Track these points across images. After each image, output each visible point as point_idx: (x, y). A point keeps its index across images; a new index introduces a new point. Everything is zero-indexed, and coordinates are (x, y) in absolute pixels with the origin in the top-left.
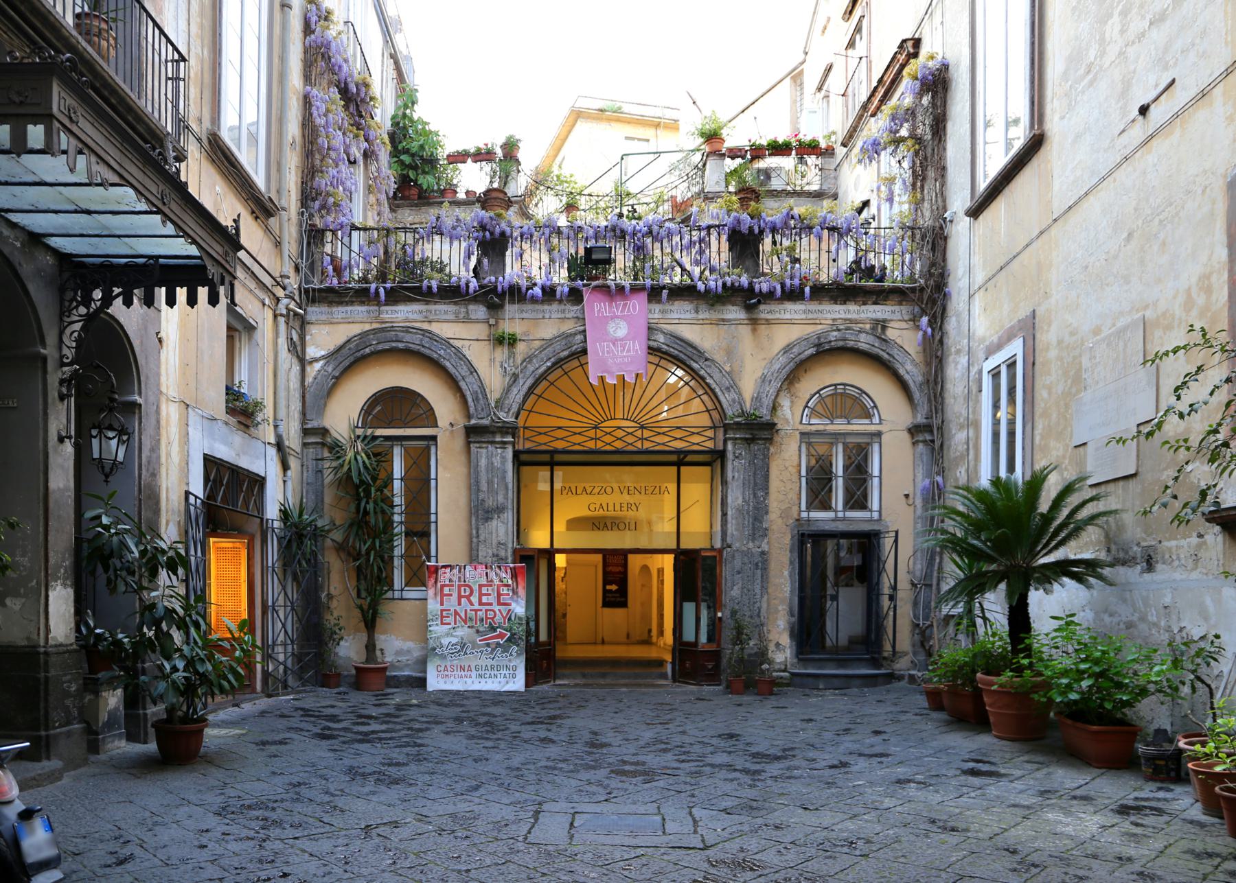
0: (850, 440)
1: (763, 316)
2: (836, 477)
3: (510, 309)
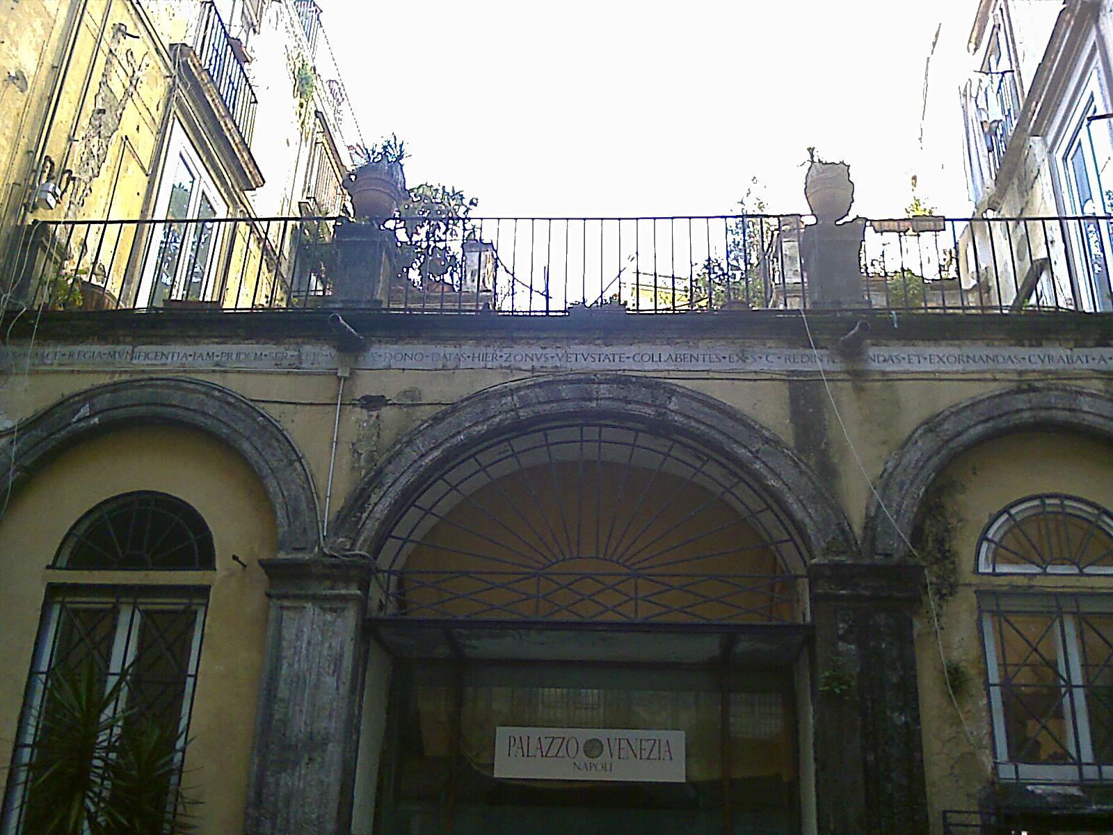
0: (1088, 607)
1: (875, 366)
2: (1070, 687)
3: (382, 353)
